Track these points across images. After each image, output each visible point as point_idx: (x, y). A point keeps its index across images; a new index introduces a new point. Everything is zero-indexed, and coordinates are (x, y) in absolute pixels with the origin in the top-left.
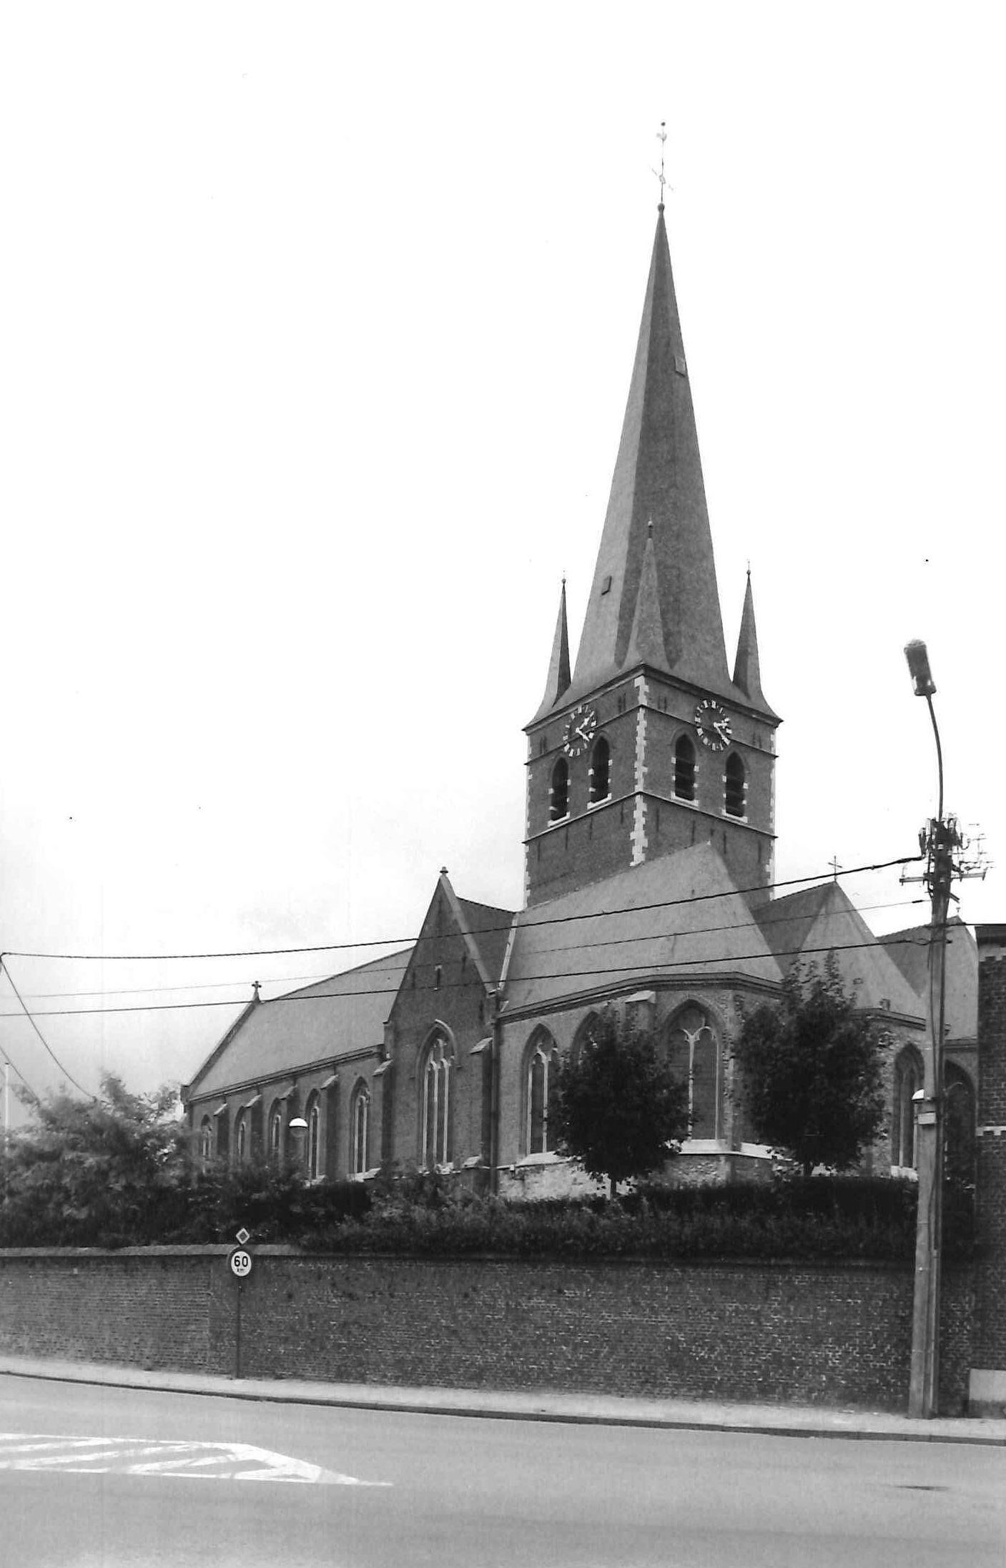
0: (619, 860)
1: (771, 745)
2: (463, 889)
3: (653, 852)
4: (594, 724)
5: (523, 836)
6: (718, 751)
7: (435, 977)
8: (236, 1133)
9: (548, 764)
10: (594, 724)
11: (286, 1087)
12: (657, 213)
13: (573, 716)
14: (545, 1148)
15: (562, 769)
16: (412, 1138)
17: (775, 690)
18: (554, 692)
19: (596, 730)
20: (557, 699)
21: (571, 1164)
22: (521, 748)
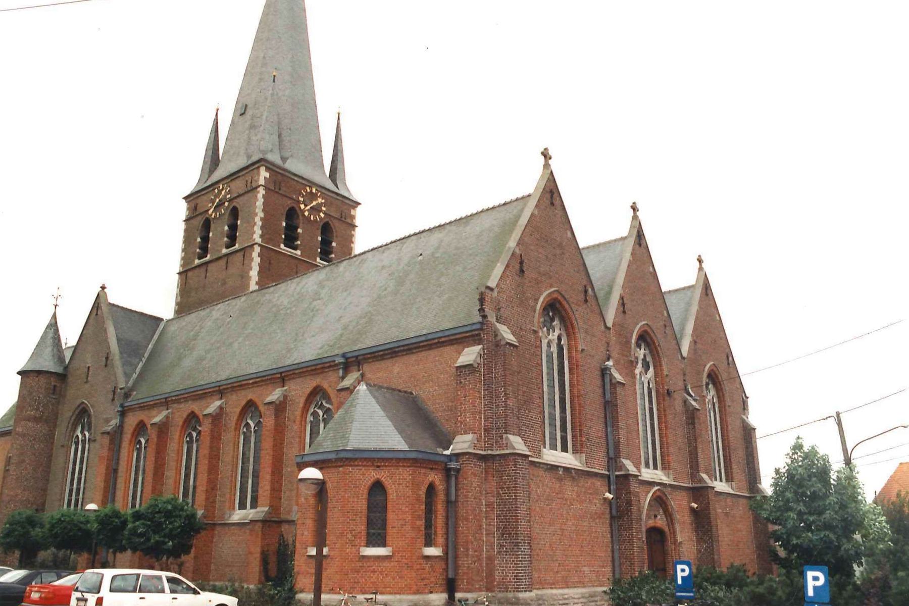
0: (240, 289)
1: (353, 217)
2: (114, 297)
3: (263, 284)
4: (229, 196)
6: (315, 221)
7: (86, 370)
8: (237, 428)
9: (198, 222)
11: (160, 412)
13: (216, 191)
16: (201, 454)
17: (355, 184)
19: (230, 200)
22: (182, 210)
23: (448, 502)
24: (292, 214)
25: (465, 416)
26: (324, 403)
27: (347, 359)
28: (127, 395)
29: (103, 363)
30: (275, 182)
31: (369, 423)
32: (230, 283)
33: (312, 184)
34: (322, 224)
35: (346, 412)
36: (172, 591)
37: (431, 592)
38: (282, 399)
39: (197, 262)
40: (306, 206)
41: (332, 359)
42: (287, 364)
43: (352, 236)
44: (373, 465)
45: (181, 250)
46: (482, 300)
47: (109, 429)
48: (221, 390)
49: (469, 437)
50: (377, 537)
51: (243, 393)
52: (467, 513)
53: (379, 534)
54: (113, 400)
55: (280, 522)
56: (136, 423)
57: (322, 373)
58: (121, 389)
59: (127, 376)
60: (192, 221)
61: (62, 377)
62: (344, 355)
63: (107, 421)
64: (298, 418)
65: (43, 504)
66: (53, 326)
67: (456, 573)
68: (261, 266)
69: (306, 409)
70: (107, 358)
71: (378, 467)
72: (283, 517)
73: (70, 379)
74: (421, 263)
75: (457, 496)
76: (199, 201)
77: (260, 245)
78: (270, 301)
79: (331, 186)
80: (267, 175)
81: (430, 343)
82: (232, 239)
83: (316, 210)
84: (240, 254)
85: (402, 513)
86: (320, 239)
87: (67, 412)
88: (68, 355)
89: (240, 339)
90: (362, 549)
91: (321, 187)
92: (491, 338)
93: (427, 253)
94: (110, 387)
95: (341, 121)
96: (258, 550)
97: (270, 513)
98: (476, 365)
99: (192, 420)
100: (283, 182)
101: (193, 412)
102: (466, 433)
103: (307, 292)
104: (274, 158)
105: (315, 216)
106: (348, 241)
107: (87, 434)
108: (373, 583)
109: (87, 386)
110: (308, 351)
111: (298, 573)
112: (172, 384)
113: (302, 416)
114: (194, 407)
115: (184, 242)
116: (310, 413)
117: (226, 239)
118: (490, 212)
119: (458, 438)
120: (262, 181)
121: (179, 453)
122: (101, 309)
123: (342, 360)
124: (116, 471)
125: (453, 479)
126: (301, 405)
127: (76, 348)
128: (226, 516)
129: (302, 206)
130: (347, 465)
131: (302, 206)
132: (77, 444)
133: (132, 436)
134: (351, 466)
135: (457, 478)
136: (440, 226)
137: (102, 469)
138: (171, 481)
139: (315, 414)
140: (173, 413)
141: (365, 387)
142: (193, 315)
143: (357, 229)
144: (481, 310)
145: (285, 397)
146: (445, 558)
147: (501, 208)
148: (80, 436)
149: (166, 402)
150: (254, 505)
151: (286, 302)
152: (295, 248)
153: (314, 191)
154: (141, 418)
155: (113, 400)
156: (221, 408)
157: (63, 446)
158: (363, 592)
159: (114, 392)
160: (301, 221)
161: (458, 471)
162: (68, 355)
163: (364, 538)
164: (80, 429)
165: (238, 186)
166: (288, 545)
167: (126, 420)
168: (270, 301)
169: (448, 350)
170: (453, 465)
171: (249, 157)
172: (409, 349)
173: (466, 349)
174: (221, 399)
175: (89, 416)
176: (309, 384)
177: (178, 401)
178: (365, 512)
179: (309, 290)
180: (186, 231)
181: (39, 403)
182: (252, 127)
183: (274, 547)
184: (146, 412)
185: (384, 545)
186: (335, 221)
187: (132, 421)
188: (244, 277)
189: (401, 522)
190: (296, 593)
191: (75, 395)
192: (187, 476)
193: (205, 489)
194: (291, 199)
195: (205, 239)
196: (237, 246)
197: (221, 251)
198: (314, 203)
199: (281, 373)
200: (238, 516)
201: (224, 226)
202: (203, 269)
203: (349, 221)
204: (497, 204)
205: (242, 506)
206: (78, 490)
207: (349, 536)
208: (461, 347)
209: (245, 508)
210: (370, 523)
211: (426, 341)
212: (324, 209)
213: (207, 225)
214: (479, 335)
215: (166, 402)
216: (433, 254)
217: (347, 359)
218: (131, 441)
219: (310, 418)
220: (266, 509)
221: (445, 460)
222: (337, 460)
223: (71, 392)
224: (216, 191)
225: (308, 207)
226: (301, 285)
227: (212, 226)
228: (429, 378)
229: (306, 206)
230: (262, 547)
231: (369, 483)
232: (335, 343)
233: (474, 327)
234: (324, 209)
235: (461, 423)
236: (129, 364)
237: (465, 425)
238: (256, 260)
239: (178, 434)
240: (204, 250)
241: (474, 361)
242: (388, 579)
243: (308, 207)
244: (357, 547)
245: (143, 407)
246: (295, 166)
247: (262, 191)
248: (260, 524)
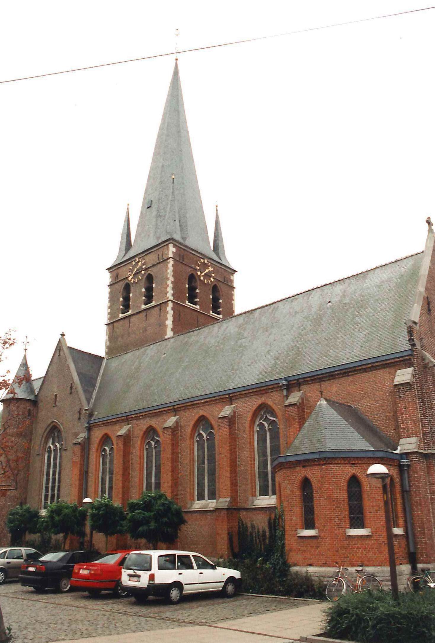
0: (158, 337)
1: (232, 281)
2: (71, 342)
5: (106, 321)
7: (54, 397)
9: (120, 286)
10: (144, 267)
12: (175, 61)
14: (258, 494)
15: (127, 288)
17: (232, 257)
18: (124, 253)
19: (146, 269)
20: (124, 257)
21: (180, 530)
22: (107, 278)
23: (404, 492)
24: (192, 278)
25: (407, 424)
26: (268, 416)
27: (289, 382)
28: (91, 415)
29: (69, 391)
30: (180, 255)
31: (331, 430)
32: (150, 330)
33: (205, 256)
34: (213, 285)
35: (314, 421)
36: (199, 568)
37: (401, 564)
38: (232, 414)
39: (121, 316)
40: (201, 273)
41: (276, 382)
42: (231, 387)
43: (233, 295)
44: (350, 463)
45: (107, 308)
46: (410, 332)
47: (79, 441)
48: (175, 409)
49: (414, 439)
50: (357, 521)
51: (196, 410)
52: (420, 500)
53: (358, 518)
54: (79, 419)
55: (239, 510)
56: (100, 436)
57: (266, 393)
58: (85, 410)
59: (88, 401)
60: (116, 286)
61: (35, 403)
62: (286, 379)
63: (76, 435)
64: (247, 428)
65: (26, 499)
66: (25, 365)
67: (415, 548)
68: (174, 316)
69: (253, 421)
70: (71, 388)
71: (353, 464)
72: (240, 505)
73: (41, 405)
74: (332, 308)
75: (410, 486)
76: (120, 271)
77: (172, 301)
78: (198, 342)
79: (215, 257)
80: (174, 250)
81: (364, 367)
82: (149, 298)
83: (208, 276)
84: (157, 309)
85: (373, 501)
86: (211, 297)
87: (41, 429)
88: (37, 386)
89: (180, 371)
90: (347, 530)
91: (211, 259)
92: (420, 361)
93: (335, 300)
94: (77, 408)
95: (218, 212)
96: (225, 532)
97: (231, 503)
98: (412, 383)
99: (151, 431)
100: (186, 255)
101: (151, 426)
102: (409, 437)
103: (230, 333)
104: (177, 237)
105: (207, 281)
106: (230, 299)
107: (57, 444)
108: (359, 558)
109: (55, 409)
110: (250, 375)
111: (290, 550)
112: (129, 404)
113: (250, 427)
114: (153, 422)
115: (109, 301)
116: (256, 426)
117: (144, 298)
118: (383, 268)
119: (402, 441)
120: (171, 255)
121: (141, 458)
122: (62, 352)
123: (285, 383)
124: (87, 472)
125: (406, 472)
126: (249, 419)
127: (45, 379)
128: (189, 506)
129: (199, 273)
130: (329, 464)
131: (199, 273)
132: (50, 452)
133: (98, 446)
134: (331, 464)
135: (408, 473)
136: (348, 278)
137: (76, 471)
138: (137, 479)
139: (261, 425)
140: (133, 427)
141: (325, 402)
142: (129, 355)
143: (235, 289)
144: (411, 340)
145: (234, 412)
146: (406, 536)
147: (393, 265)
148: (52, 447)
149: (126, 419)
150: (213, 495)
151: (213, 341)
152: (195, 304)
153: (206, 262)
154: (105, 432)
155: (79, 419)
156: (177, 422)
157: (38, 455)
158: (353, 565)
159: (80, 413)
160: (199, 284)
161: (408, 466)
162: (37, 386)
163: (348, 521)
164: (51, 441)
165: (152, 259)
166: (247, 527)
167: (92, 433)
168: (198, 342)
169: (381, 374)
170: (405, 462)
171: (158, 238)
172: (345, 373)
173: (398, 371)
174: (175, 416)
175: (59, 431)
176: (255, 402)
177: (137, 418)
178: (346, 500)
179: (232, 331)
180: (111, 293)
181: (19, 423)
182: (158, 216)
183: (236, 529)
184: (110, 427)
185: (363, 527)
186: (220, 284)
187: (97, 434)
188: (162, 326)
189: (376, 508)
190: (290, 566)
191: (46, 416)
192: (149, 475)
193: (170, 484)
194: (191, 267)
195: (127, 299)
196: (153, 303)
197: (140, 307)
198: (207, 271)
199: (229, 394)
200: (198, 505)
201: (141, 289)
202: (127, 321)
203: (229, 284)
204: (388, 262)
205: (201, 497)
206: (53, 487)
207: (336, 520)
208: (392, 370)
209: (203, 499)
210: (351, 511)
211: (361, 366)
212: (213, 275)
213: (127, 288)
214: (410, 359)
215: (126, 419)
216: (340, 301)
217: (289, 382)
218: (97, 450)
219: (257, 428)
220: (228, 499)
221: (398, 457)
222: (320, 459)
223: (42, 414)
224: (134, 263)
225: (203, 274)
226: (223, 329)
227: (132, 288)
228: (369, 393)
229: (201, 273)
230: (228, 529)
231: (347, 478)
232: (272, 370)
233: (405, 354)
234: (213, 275)
235: (404, 429)
236: (88, 393)
237: (408, 430)
238: (171, 312)
239: (139, 442)
240: (127, 307)
241: (411, 380)
242: (370, 554)
243: (203, 274)
244: (344, 529)
245: (106, 423)
246: (193, 242)
247: (171, 262)
248: (225, 512)
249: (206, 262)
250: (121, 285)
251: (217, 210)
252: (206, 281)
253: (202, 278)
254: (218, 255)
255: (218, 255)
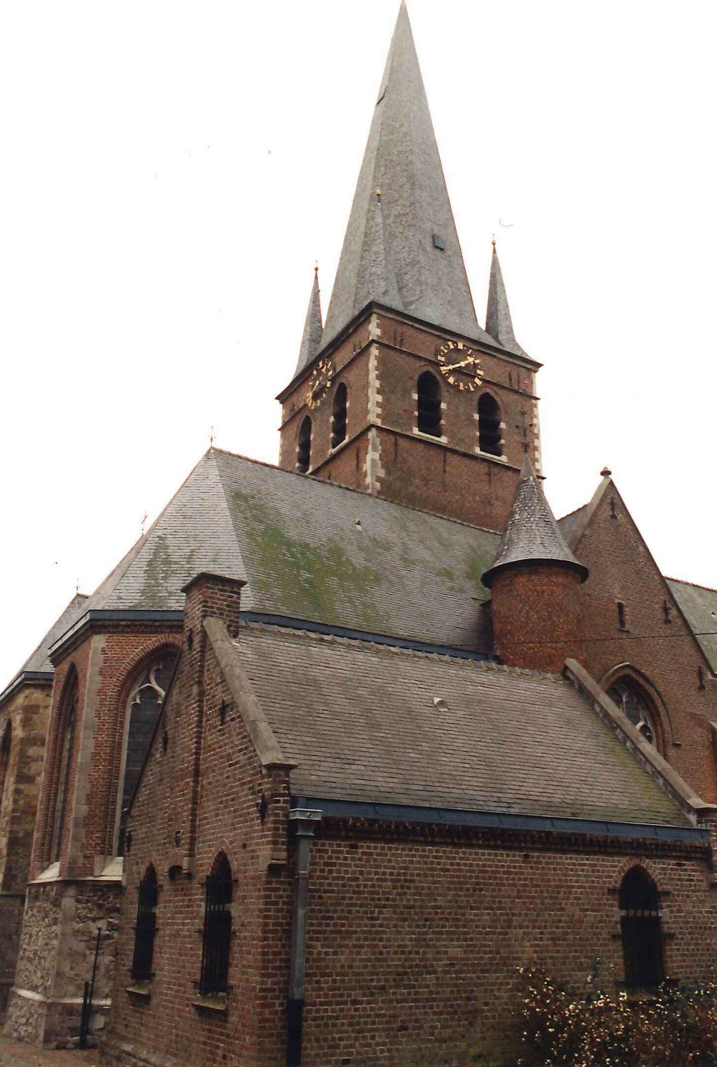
17: (527, 338)
22: (276, 413)
82: (340, 430)
95: (498, 254)
105: (466, 384)
195: (305, 446)
249: (460, 346)
250: (299, 421)
251: (494, 252)
252: (461, 385)
253: (451, 380)
254: (496, 338)
255: (496, 338)
